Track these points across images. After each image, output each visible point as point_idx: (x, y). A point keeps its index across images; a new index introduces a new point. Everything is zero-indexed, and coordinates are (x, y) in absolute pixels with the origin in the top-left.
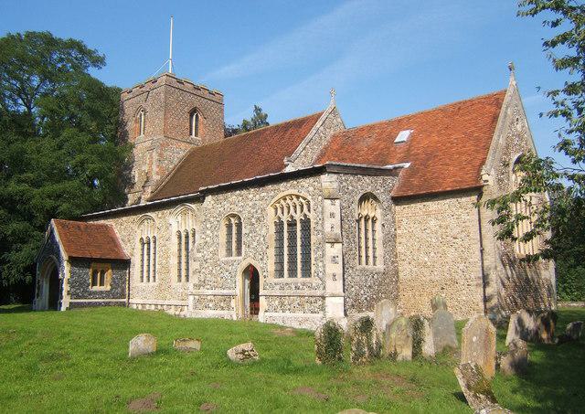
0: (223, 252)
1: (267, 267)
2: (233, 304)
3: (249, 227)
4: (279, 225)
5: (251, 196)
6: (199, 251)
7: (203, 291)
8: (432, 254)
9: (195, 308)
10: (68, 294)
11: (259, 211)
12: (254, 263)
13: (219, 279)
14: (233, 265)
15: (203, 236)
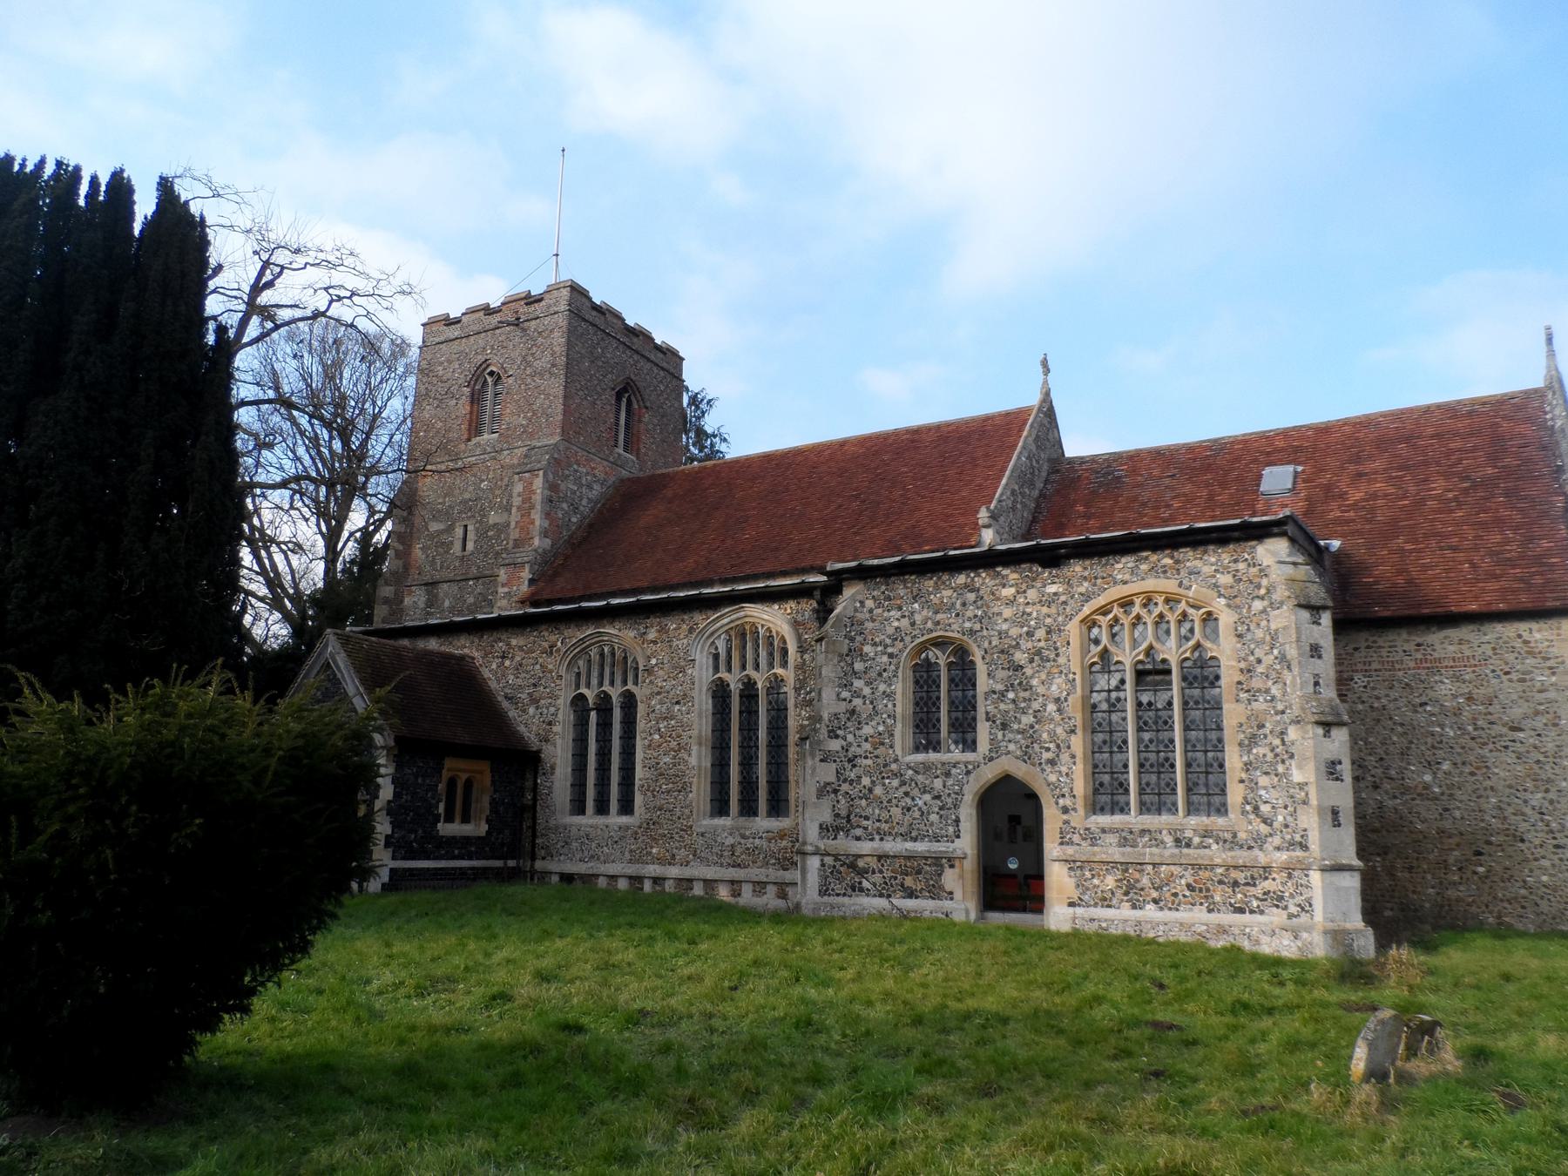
0: (902, 735)
1: (1062, 785)
2: (950, 879)
3: (1001, 674)
4: (720, 693)
5: (1008, 592)
6: (833, 735)
7: (845, 844)
8: (1446, 766)
9: (824, 892)
10: (387, 845)
11: (1041, 633)
12: (1020, 770)
13: (896, 811)
14: (948, 774)
15: (845, 694)
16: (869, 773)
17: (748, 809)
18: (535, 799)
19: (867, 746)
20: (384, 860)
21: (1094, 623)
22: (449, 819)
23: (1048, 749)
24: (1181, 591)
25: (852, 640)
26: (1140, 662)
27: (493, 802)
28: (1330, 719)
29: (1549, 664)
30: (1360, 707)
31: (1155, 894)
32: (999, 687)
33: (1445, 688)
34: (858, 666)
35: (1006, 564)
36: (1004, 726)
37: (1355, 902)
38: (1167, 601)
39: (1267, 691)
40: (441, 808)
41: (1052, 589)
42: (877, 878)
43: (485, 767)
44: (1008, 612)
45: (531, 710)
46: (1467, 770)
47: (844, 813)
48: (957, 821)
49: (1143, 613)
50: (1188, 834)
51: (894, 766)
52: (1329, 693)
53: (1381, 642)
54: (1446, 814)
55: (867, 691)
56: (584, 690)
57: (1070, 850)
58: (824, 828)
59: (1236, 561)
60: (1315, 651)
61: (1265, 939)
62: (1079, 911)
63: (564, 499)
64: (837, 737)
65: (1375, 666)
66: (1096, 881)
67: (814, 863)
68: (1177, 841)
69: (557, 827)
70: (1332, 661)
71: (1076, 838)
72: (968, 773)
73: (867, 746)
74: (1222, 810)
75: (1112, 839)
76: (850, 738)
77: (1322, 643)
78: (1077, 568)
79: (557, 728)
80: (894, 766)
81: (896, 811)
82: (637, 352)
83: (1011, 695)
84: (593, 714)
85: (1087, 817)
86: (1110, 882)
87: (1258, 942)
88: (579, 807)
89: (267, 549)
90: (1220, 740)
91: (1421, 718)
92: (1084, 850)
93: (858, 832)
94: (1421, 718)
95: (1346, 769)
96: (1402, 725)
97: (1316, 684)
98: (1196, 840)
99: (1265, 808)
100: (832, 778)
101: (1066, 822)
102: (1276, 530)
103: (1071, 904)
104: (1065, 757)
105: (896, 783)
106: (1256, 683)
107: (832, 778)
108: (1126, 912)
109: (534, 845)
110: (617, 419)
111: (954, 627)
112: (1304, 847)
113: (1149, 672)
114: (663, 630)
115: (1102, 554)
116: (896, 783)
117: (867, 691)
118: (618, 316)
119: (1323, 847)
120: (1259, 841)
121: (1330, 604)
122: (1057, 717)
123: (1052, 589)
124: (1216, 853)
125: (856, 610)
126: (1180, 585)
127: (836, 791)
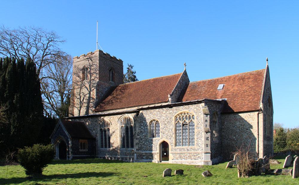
3: (163, 125)
5: (164, 112)
8: (237, 136)
11: (169, 119)
12: (166, 140)
13: (148, 147)
16: (144, 141)
17: (128, 147)
18: (95, 145)
19: (144, 137)
20: (71, 155)
21: (177, 117)
22: (81, 149)
23: (170, 137)
24: (189, 112)
25: (141, 120)
26: (183, 123)
27: (88, 146)
28: (207, 131)
29: (253, 119)
30: (226, 127)
31: (184, 158)
32: (163, 127)
33: (238, 123)
34: (142, 124)
35: (164, 108)
36: (164, 133)
37: (210, 157)
38: (187, 113)
39: (200, 127)
40: (80, 147)
41: (171, 111)
42: (145, 157)
43: (86, 141)
44: (164, 115)
45: (94, 131)
46: (240, 136)
47: (140, 147)
48: (157, 148)
49: (184, 115)
50: (189, 149)
51: (148, 140)
52: (208, 127)
53: (229, 116)
54: (237, 143)
55: (143, 128)
56: (102, 128)
57: (172, 152)
58: (137, 150)
59: (197, 107)
60: (206, 121)
61: (198, 163)
62: (173, 160)
63: (100, 92)
64: (139, 136)
65: (228, 120)
66: (176, 156)
67: (135, 155)
68: (187, 150)
69: (99, 150)
70: (209, 122)
71: (173, 150)
72: (158, 141)
73: (144, 137)
74: (194, 145)
75: (178, 150)
76: (141, 136)
77: (207, 120)
78: (174, 108)
79: (98, 134)
80: (148, 140)
81: (148, 147)
82: (113, 62)
83: (165, 128)
84: (103, 132)
85: (175, 147)
86: (178, 156)
87: (197, 164)
88: (102, 147)
89: (51, 99)
90: (194, 135)
91: (234, 128)
92: (174, 152)
93: (142, 150)
94: (234, 128)
95: (209, 139)
96: (231, 130)
97: (206, 126)
98: (190, 150)
99: (199, 145)
100: (138, 142)
101: (172, 148)
102: (202, 102)
103: (173, 159)
104: (172, 138)
105: (148, 142)
106: (199, 126)
107: (138, 142)
108: (180, 160)
109: (96, 153)
110: (110, 75)
111: (156, 118)
112: (203, 150)
113: (184, 125)
114: (113, 118)
115: (178, 106)
116: (148, 142)
117: (143, 128)
118: (109, 55)
119: (205, 150)
120: (198, 149)
121: (209, 113)
122: (171, 132)
123: (171, 111)
124: (193, 151)
125: (141, 115)
126: (189, 111)
127: (139, 144)
